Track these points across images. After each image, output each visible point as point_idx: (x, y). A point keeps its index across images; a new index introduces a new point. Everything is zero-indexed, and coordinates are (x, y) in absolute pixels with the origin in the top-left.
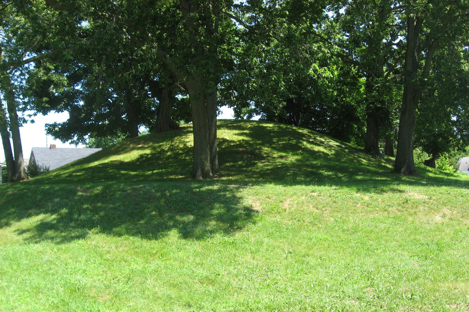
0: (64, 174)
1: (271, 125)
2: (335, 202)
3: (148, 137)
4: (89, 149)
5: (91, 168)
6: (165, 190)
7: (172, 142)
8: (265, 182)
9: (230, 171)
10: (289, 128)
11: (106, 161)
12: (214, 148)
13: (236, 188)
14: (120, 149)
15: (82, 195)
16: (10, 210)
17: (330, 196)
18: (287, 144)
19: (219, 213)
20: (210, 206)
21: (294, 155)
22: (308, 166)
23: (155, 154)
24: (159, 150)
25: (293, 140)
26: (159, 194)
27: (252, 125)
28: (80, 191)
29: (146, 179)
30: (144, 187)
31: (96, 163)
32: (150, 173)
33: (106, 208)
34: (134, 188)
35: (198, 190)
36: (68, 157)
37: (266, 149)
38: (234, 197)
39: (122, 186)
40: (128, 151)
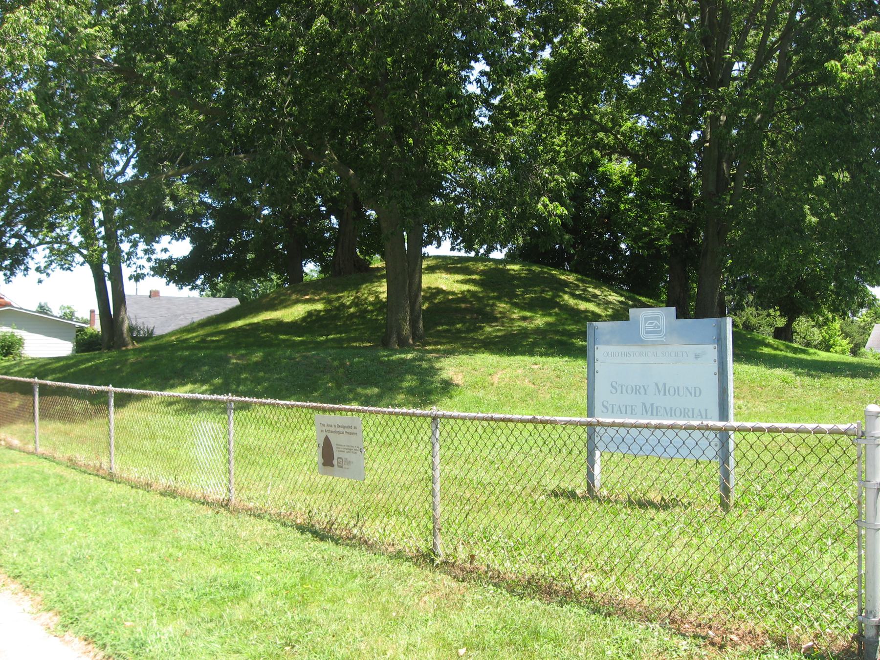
0: (193, 338)
1: (516, 267)
2: (558, 377)
3: (320, 283)
4: (212, 298)
5: (233, 330)
6: (344, 359)
7: (357, 293)
8: (475, 352)
9: (441, 337)
10: (546, 273)
11: (255, 320)
12: (418, 304)
13: (435, 357)
14: (276, 302)
15: (236, 363)
16: (143, 380)
17: (555, 370)
18: (537, 298)
19: (410, 386)
20: (399, 378)
21: (544, 315)
22: (557, 332)
23: (330, 310)
24: (336, 304)
25: (548, 291)
26: (336, 363)
27: (485, 266)
28: (232, 358)
29: (318, 346)
30: (318, 354)
31: (240, 323)
32: (323, 338)
33: (269, 378)
34: (304, 356)
35: (386, 359)
36: (179, 312)
37: (502, 306)
38: (432, 367)
39: (288, 352)
40: (289, 305)
